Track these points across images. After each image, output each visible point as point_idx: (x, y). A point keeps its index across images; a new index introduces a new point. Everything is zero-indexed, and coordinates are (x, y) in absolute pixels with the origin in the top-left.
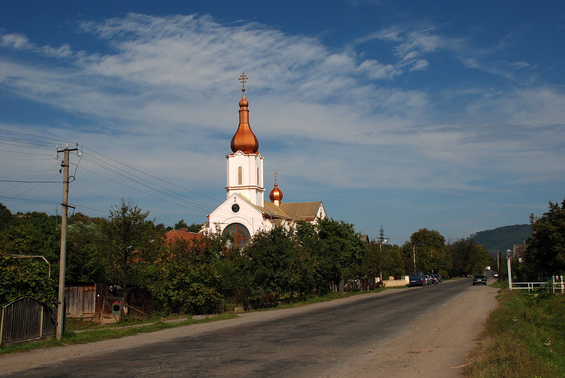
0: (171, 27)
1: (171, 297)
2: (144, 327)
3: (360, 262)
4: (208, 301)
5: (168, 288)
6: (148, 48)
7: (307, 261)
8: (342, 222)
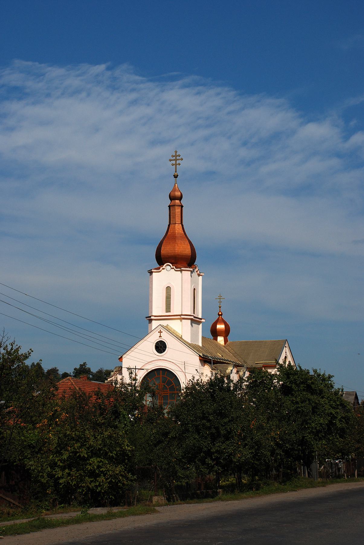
0: (74, 82)
1: (59, 478)
2: (15, 525)
3: (342, 433)
4: (114, 487)
5: (55, 464)
6: (39, 111)
7: (260, 428)
8: (315, 371)
